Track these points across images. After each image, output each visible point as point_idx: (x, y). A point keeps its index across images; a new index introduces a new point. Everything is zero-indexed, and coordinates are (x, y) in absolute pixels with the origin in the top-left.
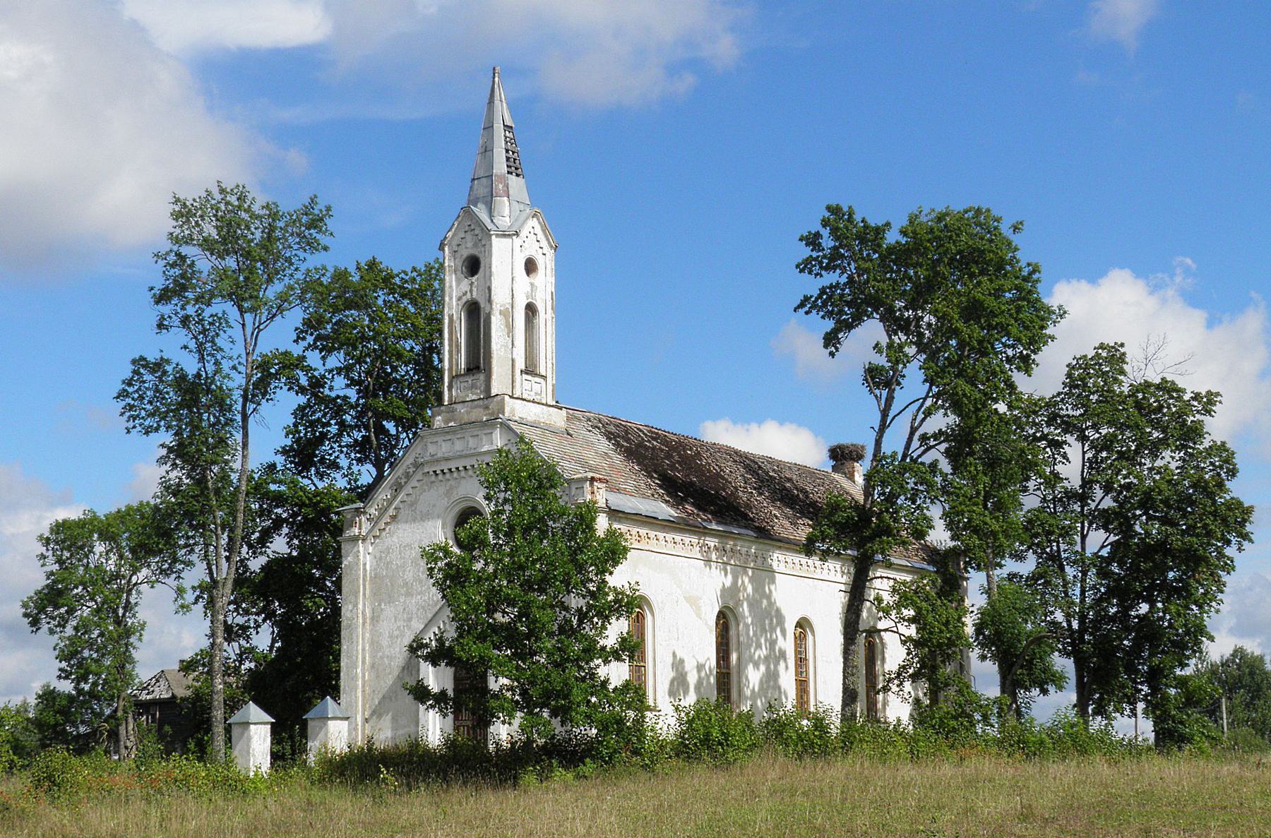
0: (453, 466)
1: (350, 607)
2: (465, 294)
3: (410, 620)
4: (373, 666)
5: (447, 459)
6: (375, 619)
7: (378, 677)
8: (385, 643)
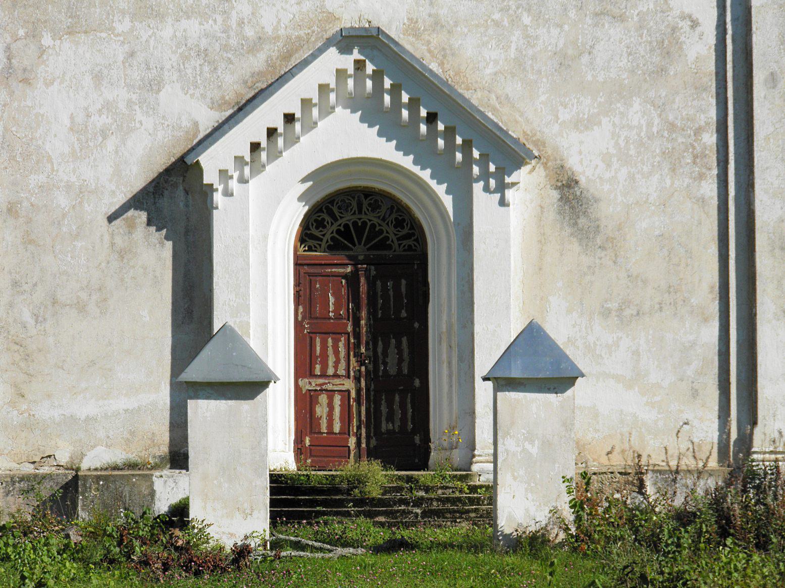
3: (154, 85)
7: (29, 240)
8: (57, 144)
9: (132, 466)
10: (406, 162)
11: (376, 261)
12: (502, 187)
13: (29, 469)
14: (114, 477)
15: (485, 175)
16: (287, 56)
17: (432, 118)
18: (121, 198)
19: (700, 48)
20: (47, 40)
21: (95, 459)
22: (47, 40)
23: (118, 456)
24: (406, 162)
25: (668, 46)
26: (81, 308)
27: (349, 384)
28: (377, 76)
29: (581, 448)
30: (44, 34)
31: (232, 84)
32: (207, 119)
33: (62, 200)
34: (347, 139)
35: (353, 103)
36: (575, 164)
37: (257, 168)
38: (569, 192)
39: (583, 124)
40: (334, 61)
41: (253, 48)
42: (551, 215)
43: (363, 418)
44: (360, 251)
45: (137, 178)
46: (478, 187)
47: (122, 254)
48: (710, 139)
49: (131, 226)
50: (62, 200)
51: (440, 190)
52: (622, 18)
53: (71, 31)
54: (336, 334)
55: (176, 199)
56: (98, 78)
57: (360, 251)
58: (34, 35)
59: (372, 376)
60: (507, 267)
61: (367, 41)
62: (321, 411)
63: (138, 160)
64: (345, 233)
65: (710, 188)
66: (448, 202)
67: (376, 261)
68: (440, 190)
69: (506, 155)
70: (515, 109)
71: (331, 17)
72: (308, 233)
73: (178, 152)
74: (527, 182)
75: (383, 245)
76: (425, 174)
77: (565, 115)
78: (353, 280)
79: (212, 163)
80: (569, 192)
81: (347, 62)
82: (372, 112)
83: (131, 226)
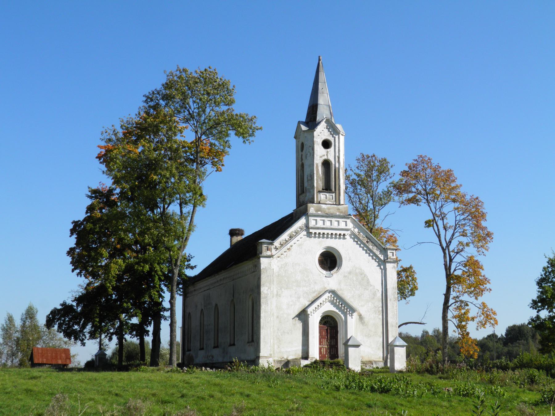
0: (326, 232)
1: (266, 288)
2: (324, 156)
3: (299, 298)
4: (278, 317)
5: (323, 229)
6: (278, 295)
9: (296, 359)
10: (337, 311)
11: (330, 326)
12: (352, 315)
13: (280, 359)
14: (295, 360)
15: (349, 313)
16: (319, 294)
17: (342, 304)
18: (294, 316)
19: (379, 295)
20: (283, 290)
21: (290, 358)
22: (283, 290)
23: (294, 357)
24: (337, 311)
25: (374, 294)
26: (288, 333)
27: (326, 346)
28: (334, 298)
29: (362, 357)
30: (19, 327)
31: (311, 298)
32: (307, 304)
33: (285, 316)
34: (328, 307)
35: (330, 301)
36: (361, 312)
37: (316, 311)
38: (360, 316)
39: (362, 306)
40: (327, 295)
41: (314, 293)
42: (358, 320)
43: (178, 338)
44: (328, 325)
45: (297, 313)
46: (348, 315)
47: (294, 325)
48: (381, 309)
49: (296, 320)
50: (285, 316)
51: (342, 316)
52: (368, 290)
53: (287, 289)
54: (325, 338)
55: (303, 316)
56: (291, 296)
57: (328, 325)
58: (281, 289)
59: (330, 345)
60: (352, 328)
61: (333, 292)
62: (322, 351)
63: (297, 310)
64: (325, 322)
65: (381, 317)
66: (343, 318)
67: (330, 326)
68: (342, 316)
69: (353, 310)
70: (354, 303)
71: (325, 288)
72: (320, 323)
73: (303, 308)
74: (355, 314)
75: (331, 324)
76: (340, 313)
77: (360, 304)
78: (327, 330)
79: (309, 310)
80: (360, 316)
81: (329, 295)
82: (332, 303)
83: (296, 320)
